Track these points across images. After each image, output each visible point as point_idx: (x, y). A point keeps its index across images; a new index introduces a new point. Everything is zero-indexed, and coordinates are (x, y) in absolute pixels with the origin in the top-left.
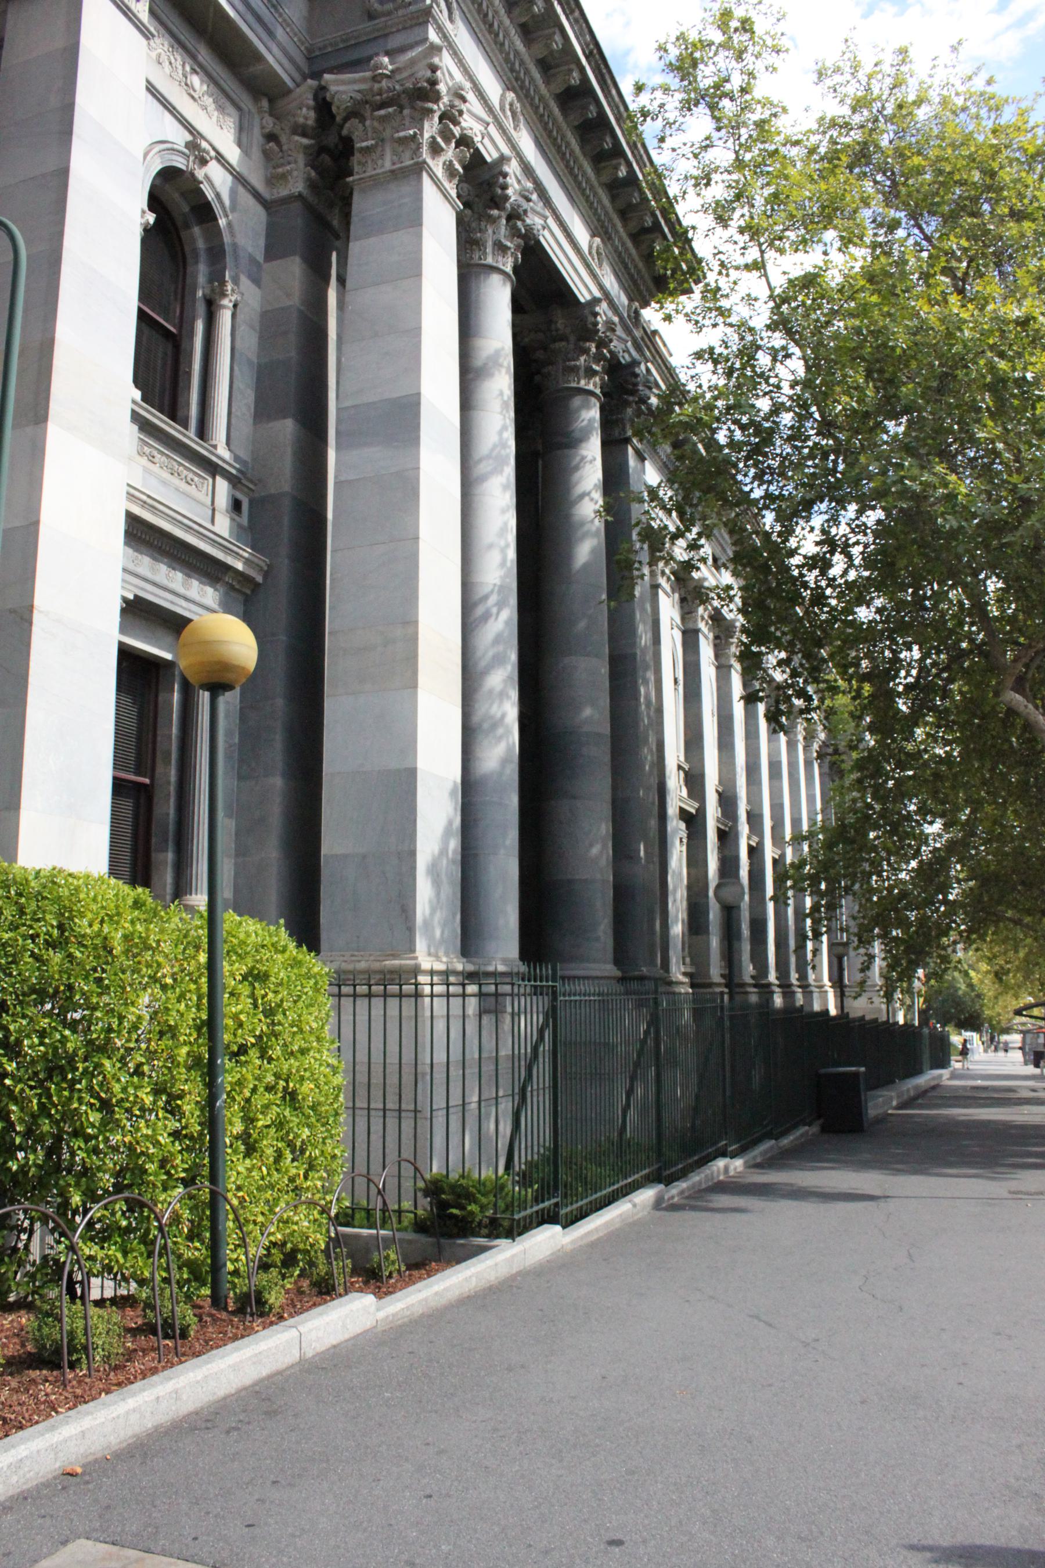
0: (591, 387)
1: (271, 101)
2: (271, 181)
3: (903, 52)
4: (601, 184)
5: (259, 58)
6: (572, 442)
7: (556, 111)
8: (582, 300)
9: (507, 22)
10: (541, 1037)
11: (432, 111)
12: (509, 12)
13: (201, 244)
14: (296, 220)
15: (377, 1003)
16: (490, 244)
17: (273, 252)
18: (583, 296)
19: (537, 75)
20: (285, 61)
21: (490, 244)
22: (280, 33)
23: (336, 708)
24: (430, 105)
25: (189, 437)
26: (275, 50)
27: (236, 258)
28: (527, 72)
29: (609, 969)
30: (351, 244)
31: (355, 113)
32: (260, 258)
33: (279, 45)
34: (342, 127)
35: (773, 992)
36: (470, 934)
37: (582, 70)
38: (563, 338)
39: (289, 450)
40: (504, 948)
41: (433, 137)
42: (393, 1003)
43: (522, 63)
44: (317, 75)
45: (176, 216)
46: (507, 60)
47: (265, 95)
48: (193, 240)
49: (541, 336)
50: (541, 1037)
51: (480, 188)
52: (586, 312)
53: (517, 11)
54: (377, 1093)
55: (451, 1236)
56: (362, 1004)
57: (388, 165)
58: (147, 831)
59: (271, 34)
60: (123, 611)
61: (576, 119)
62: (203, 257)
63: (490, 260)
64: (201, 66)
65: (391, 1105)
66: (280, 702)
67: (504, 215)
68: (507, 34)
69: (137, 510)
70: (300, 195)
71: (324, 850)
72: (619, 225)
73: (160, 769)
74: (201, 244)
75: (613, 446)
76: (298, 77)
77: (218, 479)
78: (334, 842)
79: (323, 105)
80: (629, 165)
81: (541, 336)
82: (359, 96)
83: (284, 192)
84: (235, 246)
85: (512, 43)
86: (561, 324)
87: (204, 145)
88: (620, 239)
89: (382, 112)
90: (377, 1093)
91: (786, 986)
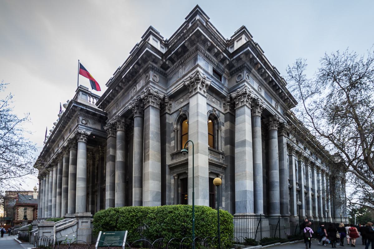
0: (276, 129)
1: (224, 99)
2: (226, 110)
3: (337, 52)
4: (277, 94)
5: (222, 93)
6: (273, 138)
7: (268, 86)
8: (274, 115)
9: (258, 75)
10: (259, 225)
11: (246, 96)
12: (258, 74)
13: (216, 123)
14: (228, 115)
15: (242, 219)
16: (257, 112)
17: (226, 121)
18: (274, 114)
19: (264, 81)
20: (225, 93)
21: (257, 112)
22: (224, 89)
23: (237, 183)
24: (245, 95)
25: (216, 150)
26: (224, 91)
27: (220, 123)
28: (262, 81)
29: (279, 215)
30: (236, 119)
31: (235, 98)
32: (224, 122)
33: (225, 91)
34: (233, 101)
35: (322, 219)
36: (255, 209)
37: (272, 78)
38: (271, 122)
39: (229, 150)
40: (261, 212)
41: (246, 100)
42: (244, 219)
43: (261, 80)
44: (229, 93)
45: (213, 117)
46: (259, 81)
47: (223, 98)
48: (215, 122)
49: (267, 122)
50: (259, 225)
51: (254, 104)
52: (275, 117)
53: (260, 73)
54: (242, 230)
55: (247, 245)
56: (240, 219)
57: (240, 106)
58: (213, 201)
59: (223, 90)
60: (209, 174)
61: (272, 85)
62: (216, 124)
63: (257, 115)
64: (214, 97)
65: (237, 231)
66: (229, 182)
67: (259, 107)
68: (258, 77)
69: (210, 161)
70: (229, 112)
71: (236, 201)
72: (281, 99)
73: (215, 192)
74: (216, 123)
75: (280, 136)
76: (227, 94)
77: (220, 155)
78: (237, 199)
79: (231, 98)
80: (281, 90)
81: (267, 122)
82: (235, 96)
83: (227, 112)
84: (220, 122)
85: (259, 78)
86: (271, 119)
87: (215, 109)
88: (281, 102)
89: (239, 98)
90: (242, 230)
91: (325, 217)
